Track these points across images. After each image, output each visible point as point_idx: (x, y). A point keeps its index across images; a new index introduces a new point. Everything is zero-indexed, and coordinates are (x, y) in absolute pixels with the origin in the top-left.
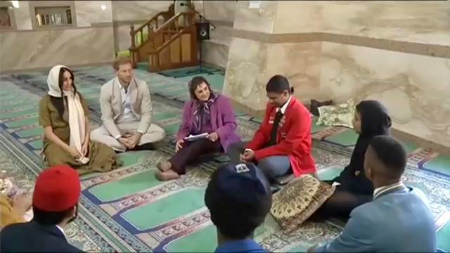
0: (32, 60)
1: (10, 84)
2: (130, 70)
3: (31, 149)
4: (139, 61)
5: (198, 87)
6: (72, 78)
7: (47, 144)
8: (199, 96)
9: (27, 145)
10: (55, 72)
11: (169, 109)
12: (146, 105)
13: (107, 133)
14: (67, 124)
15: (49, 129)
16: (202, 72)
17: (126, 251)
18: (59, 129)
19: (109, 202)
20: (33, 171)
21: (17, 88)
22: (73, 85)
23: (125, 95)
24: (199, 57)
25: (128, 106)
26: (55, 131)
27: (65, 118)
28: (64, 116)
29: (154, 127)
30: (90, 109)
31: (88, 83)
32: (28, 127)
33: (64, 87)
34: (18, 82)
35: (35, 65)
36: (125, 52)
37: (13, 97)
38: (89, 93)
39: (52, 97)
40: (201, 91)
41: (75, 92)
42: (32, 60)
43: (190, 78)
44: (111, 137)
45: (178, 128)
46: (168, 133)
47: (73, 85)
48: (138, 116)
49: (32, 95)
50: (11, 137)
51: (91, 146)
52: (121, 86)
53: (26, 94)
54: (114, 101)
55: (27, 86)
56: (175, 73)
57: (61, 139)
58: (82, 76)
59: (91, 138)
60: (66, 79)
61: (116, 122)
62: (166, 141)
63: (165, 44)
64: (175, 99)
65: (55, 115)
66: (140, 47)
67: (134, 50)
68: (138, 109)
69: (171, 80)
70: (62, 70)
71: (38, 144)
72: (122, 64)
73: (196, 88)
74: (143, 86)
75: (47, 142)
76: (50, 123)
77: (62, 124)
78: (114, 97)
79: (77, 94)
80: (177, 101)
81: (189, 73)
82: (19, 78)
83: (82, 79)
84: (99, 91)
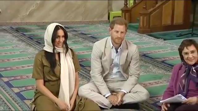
0: (31, 14)
1: (9, 36)
2: (122, 32)
3: (23, 98)
4: (130, 22)
5: (185, 48)
6: (66, 36)
7: (38, 95)
8: (185, 57)
9: (18, 94)
10: (51, 28)
11: (160, 72)
12: (133, 68)
13: (96, 90)
14: (59, 79)
15: (42, 81)
16: (193, 35)
17: (17, 110)
18: (52, 83)
19: (7, 77)
20: (6, 101)
21: (15, 40)
22: (65, 43)
23: (115, 54)
24: (192, 20)
25: (117, 65)
26: (47, 83)
27: (57, 74)
28: (56, 70)
29: (139, 88)
30: (81, 65)
31: (80, 39)
32: (21, 77)
33: (56, 44)
34: (16, 34)
35: (32, 20)
36: (117, 12)
37: (10, 47)
38: (81, 49)
39: (46, 52)
40: (187, 53)
41: (67, 48)
42: (31, 14)
43: (182, 40)
44: (101, 95)
45: (165, 90)
46: (152, 95)
47: (65, 43)
48: (125, 75)
49: (28, 47)
50: (6, 86)
51: (78, 101)
52: (112, 45)
53: (22, 45)
54: (104, 59)
55: (23, 38)
56: (165, 35)
57: (52, 92)
58: (74, 33)
59: (79, 93)
60: (59, 37)
61: (105, 79)
62: (149, 101)
63: (157, 5)
64: (163, 62)
65: (47, 69)
66: (133, 7)
67: (126, 10)
68: (126, 69)
69: (161, 42)
70: (57, 28)
71: (30, 95)
72: (117, 23)
73: (183, 49)
74: (133, 49)
75: (38, 94)
76: (42, 77)
77: (54, 78)
78: (105, 55)
79: (69, 51)
80: (164, 64)
81: (180, 36)
82: (17, 30)
83: (75, 35)
84: (91, 48)
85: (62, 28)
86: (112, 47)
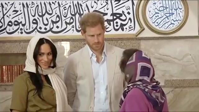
70: (41, 42)
85: (48, 41)
86: (92, 54)
